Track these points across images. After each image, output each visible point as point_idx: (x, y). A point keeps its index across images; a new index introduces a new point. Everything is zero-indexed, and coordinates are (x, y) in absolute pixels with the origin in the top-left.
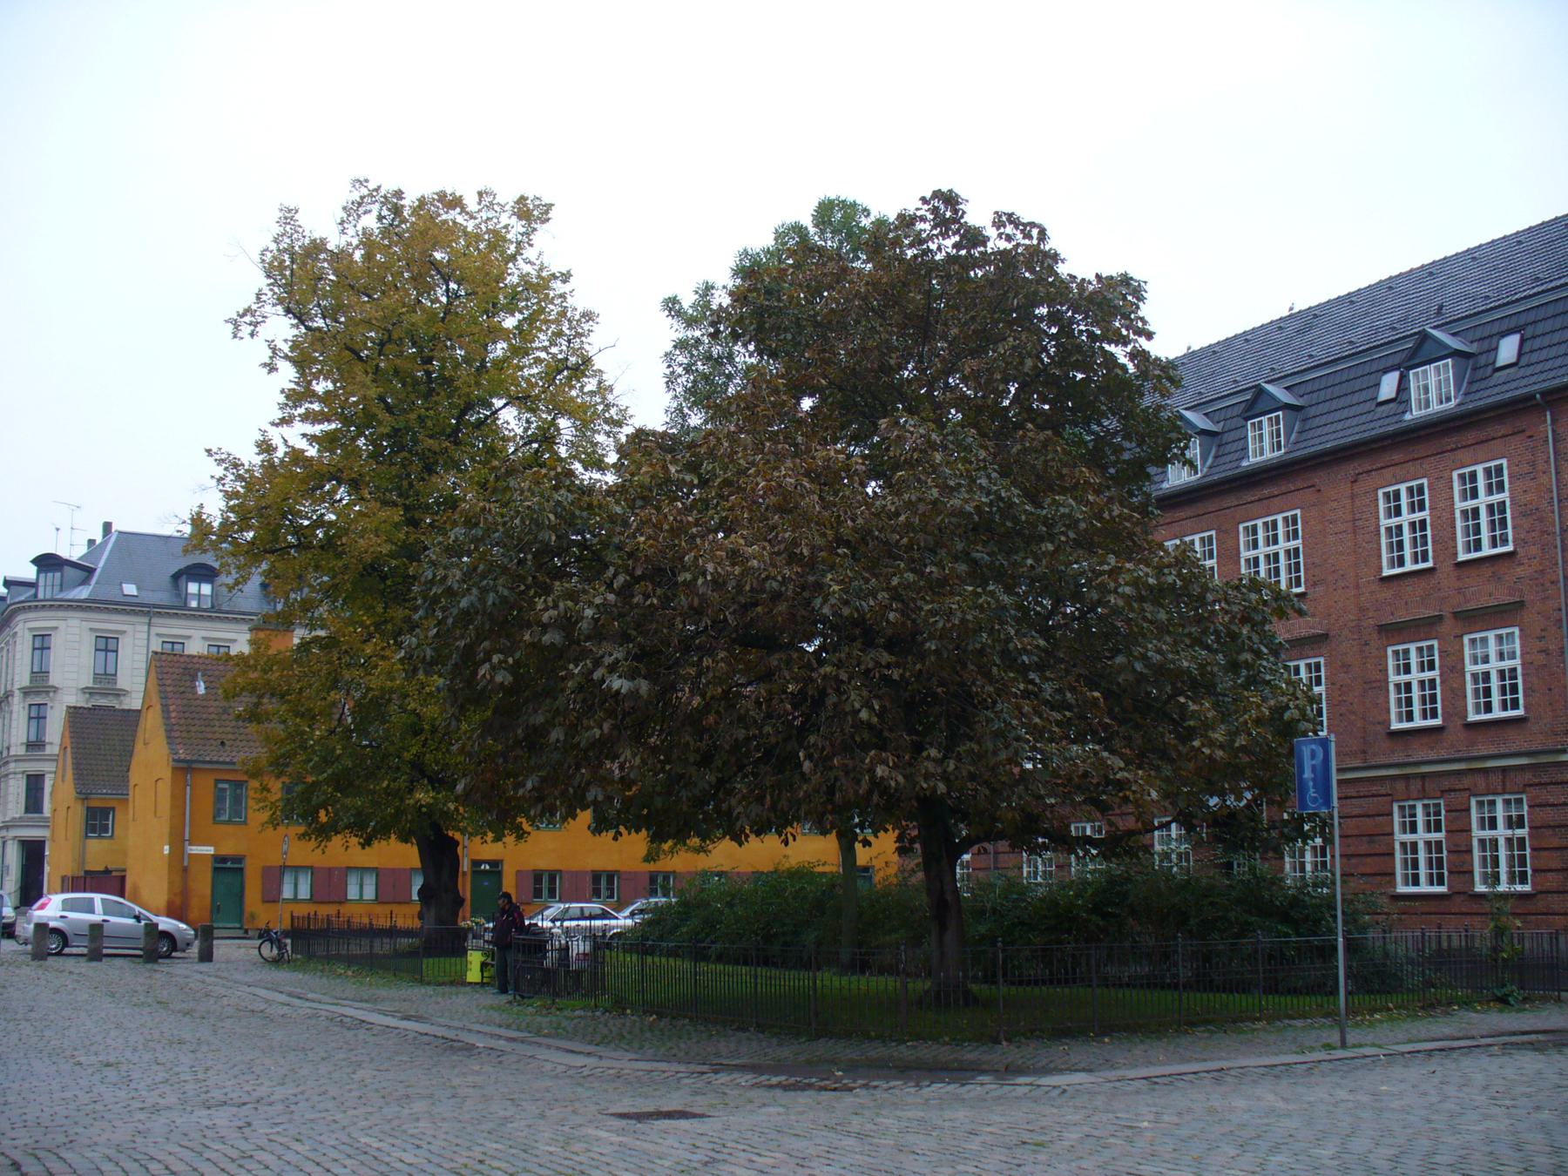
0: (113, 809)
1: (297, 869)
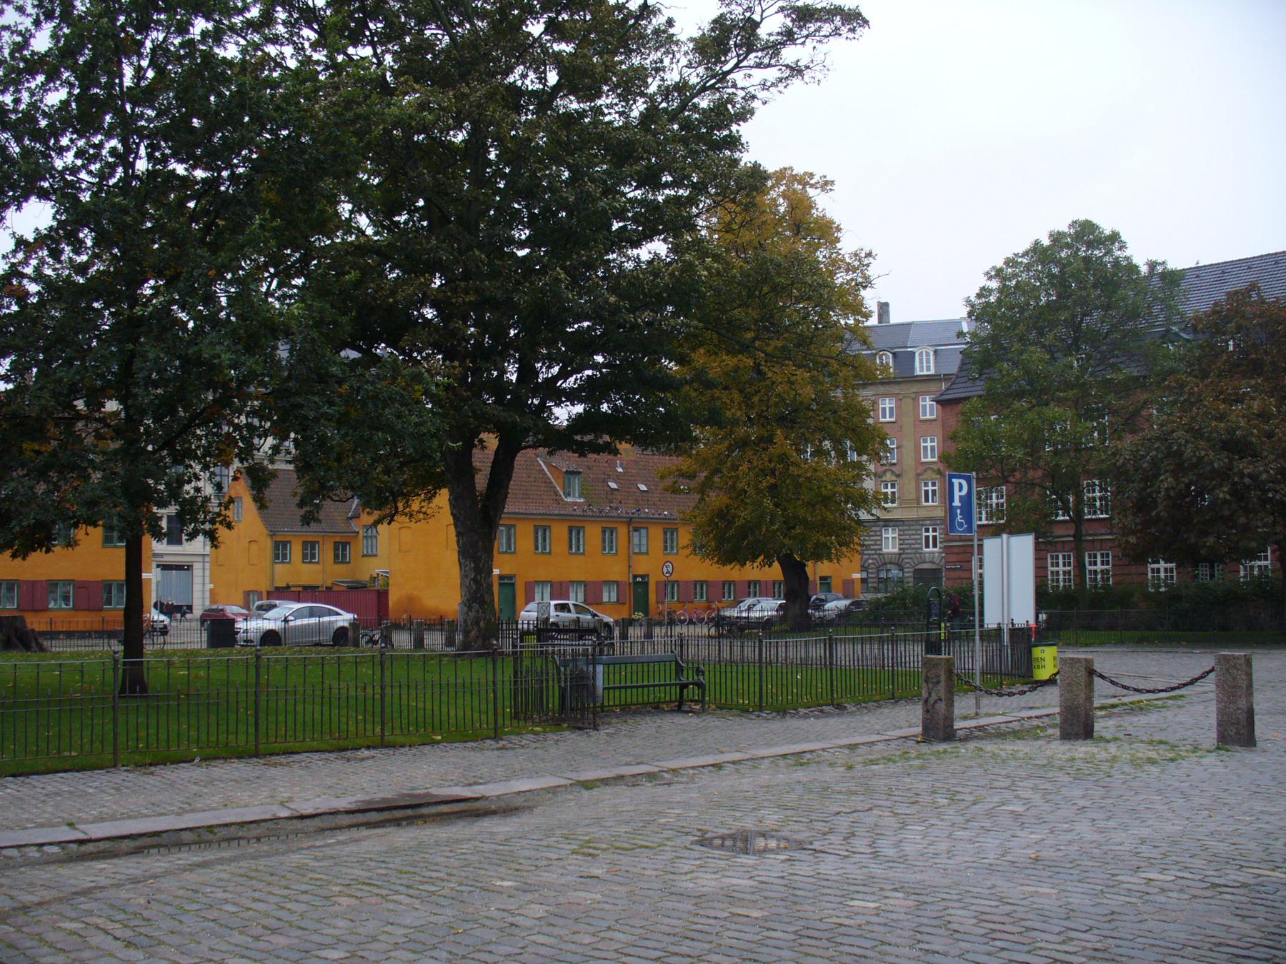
0: (290, 542)
1: (543, 583)
